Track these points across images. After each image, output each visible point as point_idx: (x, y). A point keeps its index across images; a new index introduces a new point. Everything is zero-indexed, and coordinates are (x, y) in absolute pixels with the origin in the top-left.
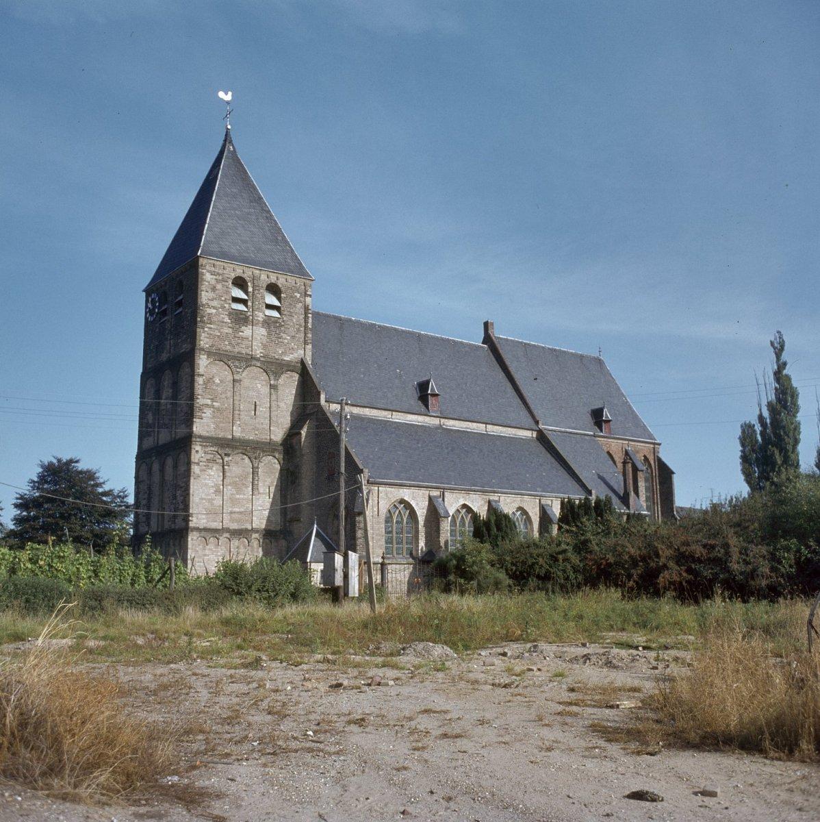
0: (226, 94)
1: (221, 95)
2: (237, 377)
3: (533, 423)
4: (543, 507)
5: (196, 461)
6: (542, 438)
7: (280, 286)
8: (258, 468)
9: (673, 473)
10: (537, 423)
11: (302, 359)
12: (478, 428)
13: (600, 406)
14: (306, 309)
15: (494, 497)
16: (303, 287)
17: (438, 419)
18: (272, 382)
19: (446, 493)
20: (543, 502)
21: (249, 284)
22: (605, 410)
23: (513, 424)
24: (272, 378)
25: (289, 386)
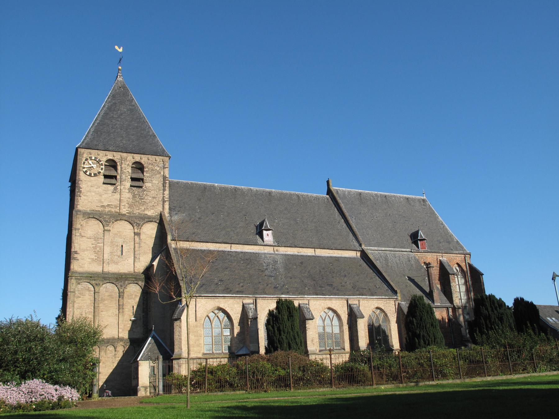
0: (120, 48)
1: (117, 47)
2: (106, 228)
3: (357, 245)
4: (350, 306)
5: (72, 290)
6: (364, 256)
7: (143, 163)
8: (123, 293)
9: (482, 274)
10: (360, 245)
11: (161, 214)
12: (309, 252)
13: (417, 229)
14: (164, 178)
15: (353, 301)
16: (162, 163)
17: (79, 222)
18: (136, 231)
19: (258, 301)
20: (350, 302)
21: (118, 164)
22: (420, 232)
23: (339, 248)
24: (136, 227)
25: (150, 231)
